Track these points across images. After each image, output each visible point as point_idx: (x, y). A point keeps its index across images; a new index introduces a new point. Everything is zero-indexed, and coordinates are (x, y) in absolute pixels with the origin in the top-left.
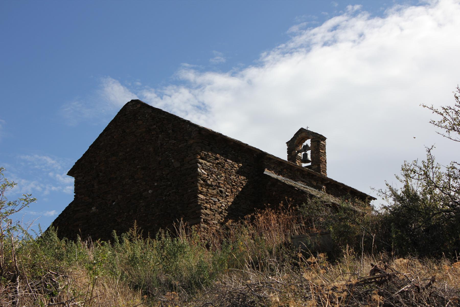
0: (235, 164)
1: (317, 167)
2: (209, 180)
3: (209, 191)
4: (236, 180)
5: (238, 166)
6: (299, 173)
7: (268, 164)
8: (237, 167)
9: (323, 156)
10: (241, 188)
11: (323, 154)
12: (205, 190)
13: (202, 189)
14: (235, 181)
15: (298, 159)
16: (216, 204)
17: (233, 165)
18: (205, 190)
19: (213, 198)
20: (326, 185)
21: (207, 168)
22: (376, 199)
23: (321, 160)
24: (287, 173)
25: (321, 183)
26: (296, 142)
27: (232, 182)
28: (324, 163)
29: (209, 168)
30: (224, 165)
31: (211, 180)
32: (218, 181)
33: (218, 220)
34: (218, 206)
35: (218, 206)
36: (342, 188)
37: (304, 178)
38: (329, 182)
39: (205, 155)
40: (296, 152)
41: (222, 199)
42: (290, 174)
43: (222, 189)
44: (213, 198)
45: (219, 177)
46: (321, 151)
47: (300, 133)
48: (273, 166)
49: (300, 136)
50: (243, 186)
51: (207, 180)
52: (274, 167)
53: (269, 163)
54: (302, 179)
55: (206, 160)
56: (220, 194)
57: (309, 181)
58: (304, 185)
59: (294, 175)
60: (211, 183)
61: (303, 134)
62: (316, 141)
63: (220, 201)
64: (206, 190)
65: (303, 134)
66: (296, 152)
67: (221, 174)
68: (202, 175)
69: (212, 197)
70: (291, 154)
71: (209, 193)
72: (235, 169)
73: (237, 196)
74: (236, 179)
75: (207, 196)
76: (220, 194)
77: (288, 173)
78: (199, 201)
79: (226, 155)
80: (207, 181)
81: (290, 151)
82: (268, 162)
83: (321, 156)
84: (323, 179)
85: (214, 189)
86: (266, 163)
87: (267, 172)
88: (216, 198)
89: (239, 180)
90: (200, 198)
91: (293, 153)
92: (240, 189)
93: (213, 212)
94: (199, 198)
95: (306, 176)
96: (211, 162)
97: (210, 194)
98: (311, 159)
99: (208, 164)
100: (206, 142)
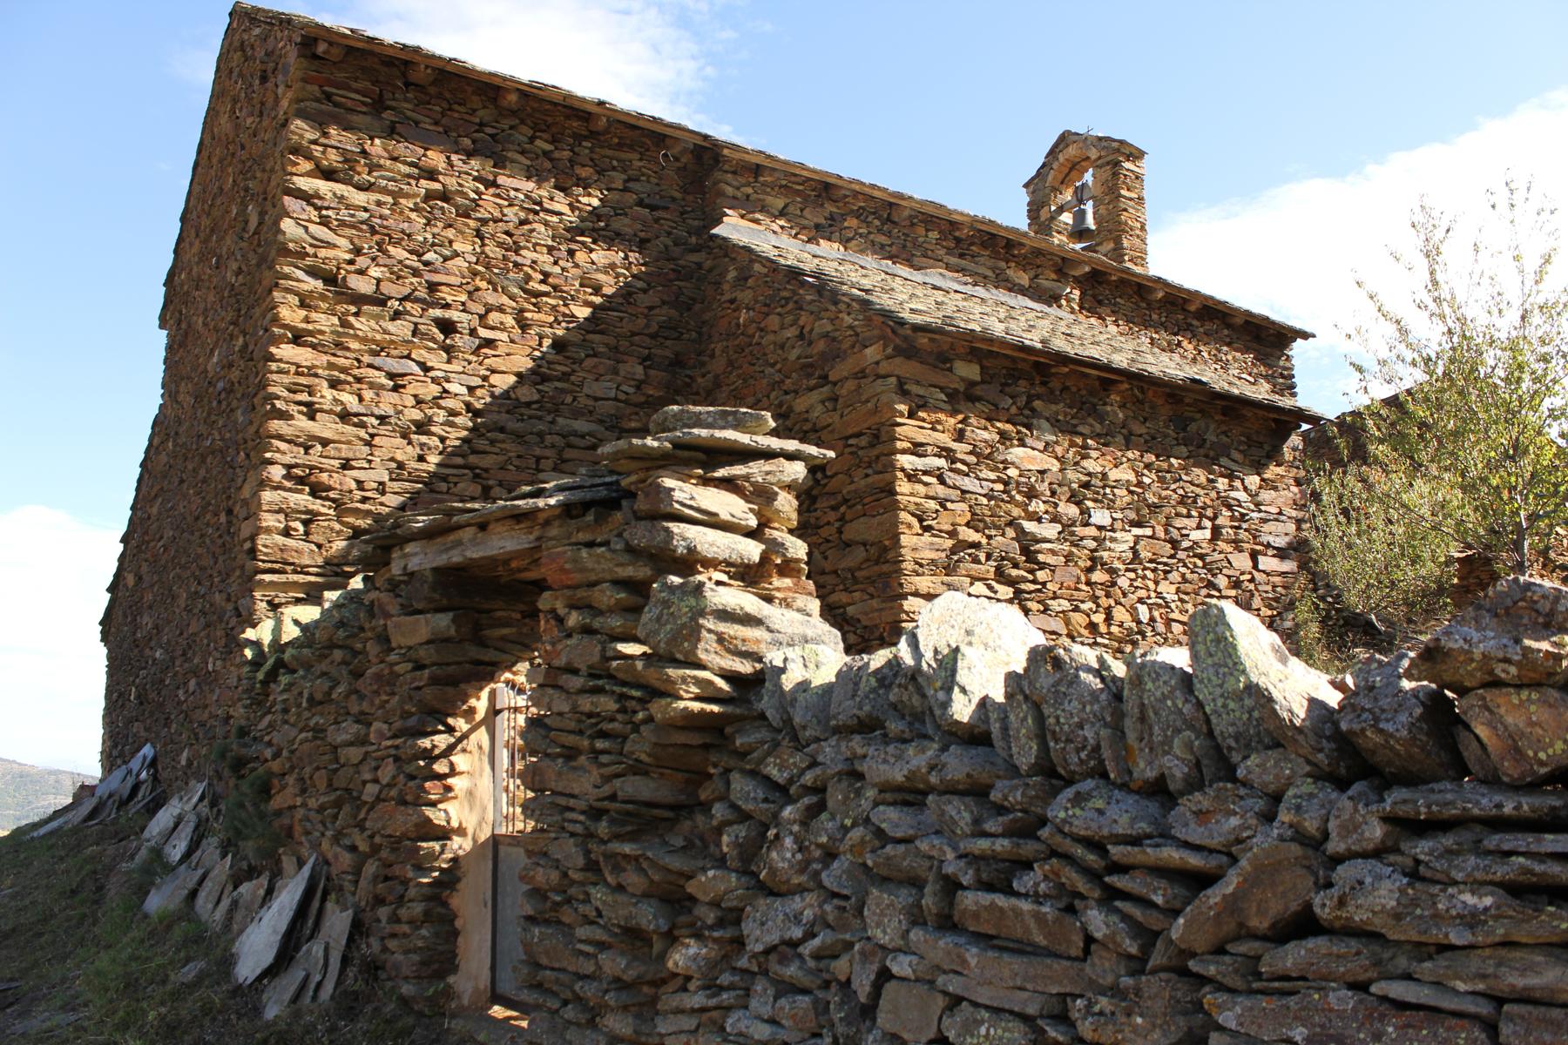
0: (552, 199)
1: (1111, 245)
2: (362, 272)
3: (351, 327)
4: (557, 270)
5: (570, 205)
6: (934, 235)
7: (748, 196)
8: (566, 210)
9: (1131, 210)
10: (587, 304)
11: (1131, 203)
12: (325, 322)
13: (307, 320)
14: (546, 275)
15: (1059, 233)
16: (404, 386)
17: (540, 204)
18: (325, 322)
19: (377, 361)
20: (1079, 282)
21: (352, 216)
22: (1314, 336)
23: (1126, 224)
24: (861, 235)
25: (1053, 276)
26: (1050, 178)
27: (528, 278)
28: (1138, 232)
29: (366, 215)
30: (474, 200)
31: (375, 272)
32: (428, 276)
33: (394, 465)
34: (415, 396)
35: (415, 396)
36: (1160, 295)
37: (961, 256)
38: (1087, 269)
39: (348, 159)
40: (1053, 208)
41: (449, 362)
42: (883, 239)
43: (455, 315)
44: (377, 361)
45: (430, 256)
46: (1124, 192)
47: (1061, 147)
48: (780, 203)
49: (1061, 158)
50: (603, 296)
51: (348, 272)
52: (786, 206)
53: (749, 190)
54: (953, 260)
55: (347, 182)
56: (434, 340)
57: (993, 269)
58: (960, 283)
59: (908, 244)
60: (378, 285)
61: (1072, 151)
62: (1108, 163)
63: (432, 369)
64: (335, 320)
65: (1072, 151)
66: (1053, 208)
67: (451, 242)
68: (310, 250)
69: (376, 354)
70: (1038, 217)
71: (356, 337)
72: (555, 219)
73: (558, 345)
74: (556, 263)
75: (339, 353)
76: (434, 340)
77: (870, 233)
78: (274, 377)
79: (494, 150)
80: (344, 278)
81: (1034, 211)
82: (748, 184)
83: (1125, 210)
84: (1063, 259)
85: (397, 315)
86: (730, 191)
87: (734, 228)
88: (408, 357)
89: (574, 271)
90: (280, 360)
91: (1044, 214)
92: (583, 313)
93: (363, 425)
94: (274, 366)
95: (973, 248)
96: (385, 191)
97: (364, 340)
98: (1095, 224)
99: (360, 198)
100: (353, 95)
